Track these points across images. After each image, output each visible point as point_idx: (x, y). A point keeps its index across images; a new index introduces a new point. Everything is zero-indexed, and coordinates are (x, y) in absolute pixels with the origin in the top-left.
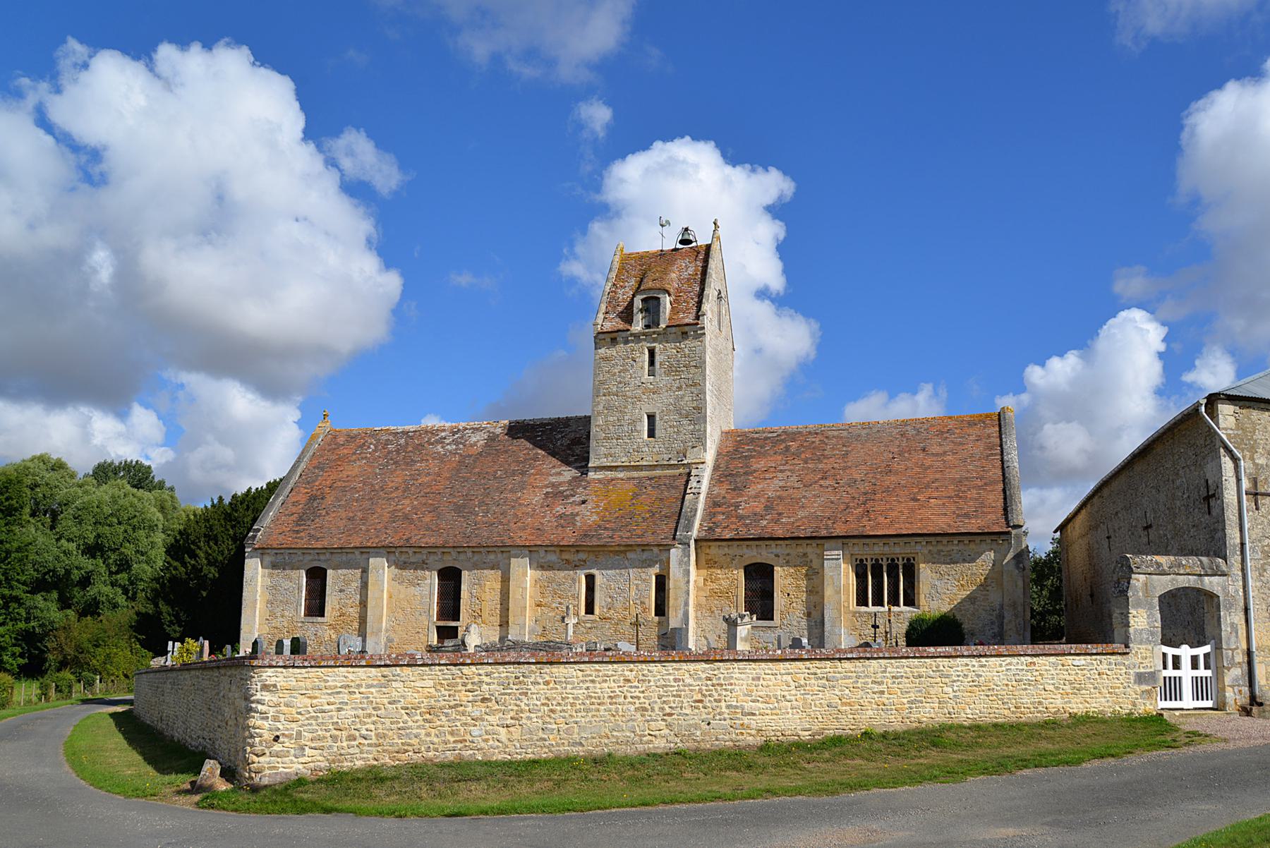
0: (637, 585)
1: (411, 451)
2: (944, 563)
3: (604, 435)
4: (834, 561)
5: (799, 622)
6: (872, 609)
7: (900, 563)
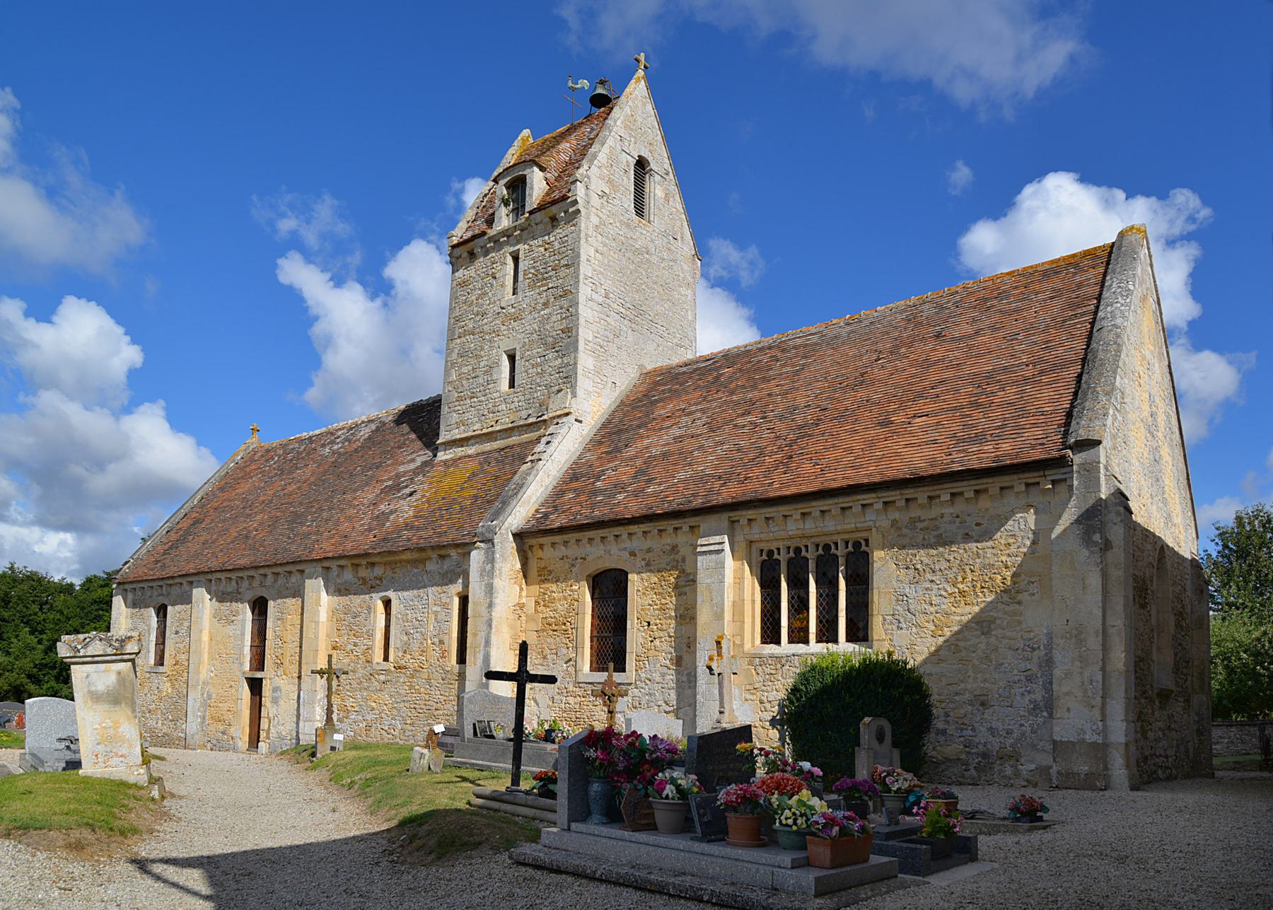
0: (436, 613)
2: (925, 546)
3: (456, 395)
4: (713, 556)
5: (663, 675)
6: (785, 647)
7: (840, 552)
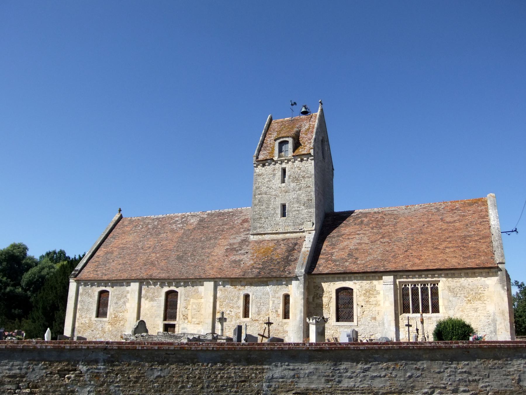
1: (159, 228)
